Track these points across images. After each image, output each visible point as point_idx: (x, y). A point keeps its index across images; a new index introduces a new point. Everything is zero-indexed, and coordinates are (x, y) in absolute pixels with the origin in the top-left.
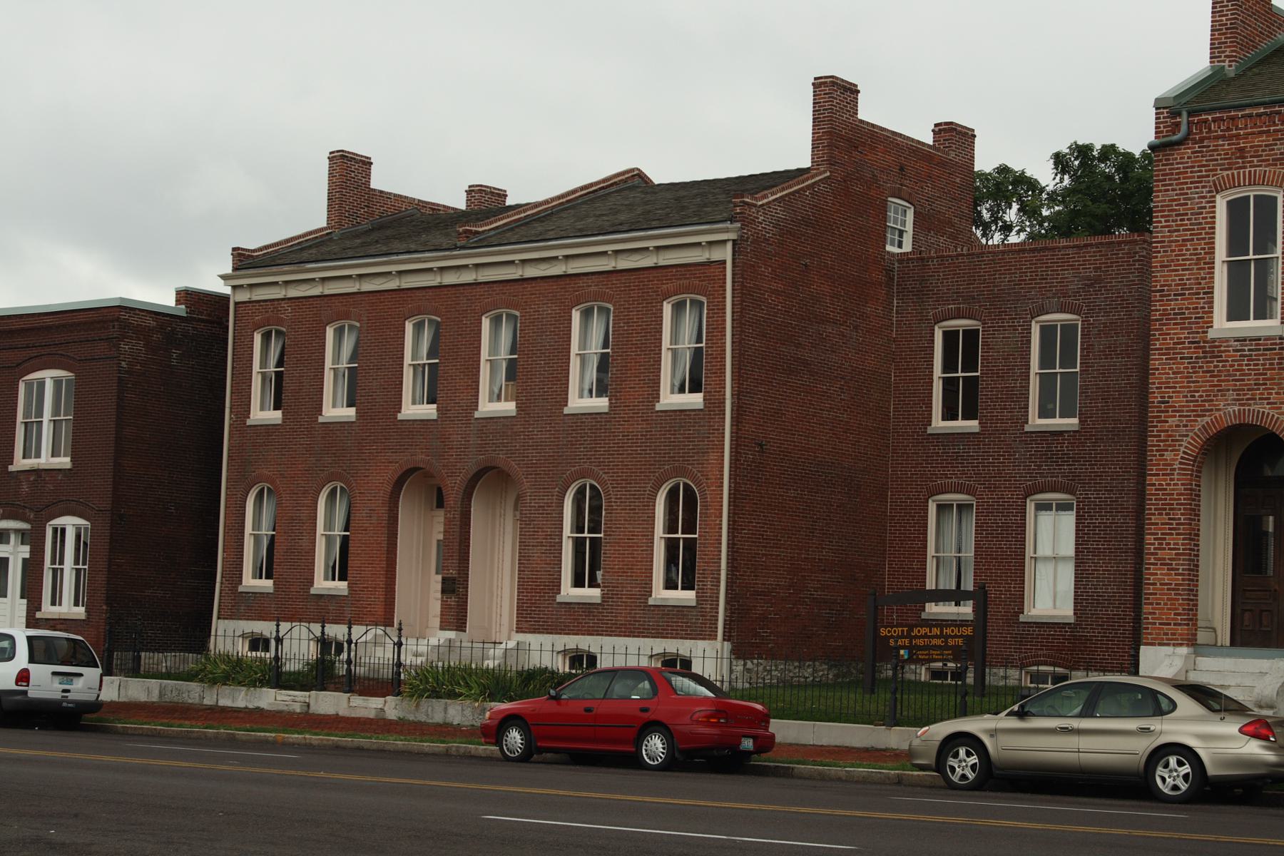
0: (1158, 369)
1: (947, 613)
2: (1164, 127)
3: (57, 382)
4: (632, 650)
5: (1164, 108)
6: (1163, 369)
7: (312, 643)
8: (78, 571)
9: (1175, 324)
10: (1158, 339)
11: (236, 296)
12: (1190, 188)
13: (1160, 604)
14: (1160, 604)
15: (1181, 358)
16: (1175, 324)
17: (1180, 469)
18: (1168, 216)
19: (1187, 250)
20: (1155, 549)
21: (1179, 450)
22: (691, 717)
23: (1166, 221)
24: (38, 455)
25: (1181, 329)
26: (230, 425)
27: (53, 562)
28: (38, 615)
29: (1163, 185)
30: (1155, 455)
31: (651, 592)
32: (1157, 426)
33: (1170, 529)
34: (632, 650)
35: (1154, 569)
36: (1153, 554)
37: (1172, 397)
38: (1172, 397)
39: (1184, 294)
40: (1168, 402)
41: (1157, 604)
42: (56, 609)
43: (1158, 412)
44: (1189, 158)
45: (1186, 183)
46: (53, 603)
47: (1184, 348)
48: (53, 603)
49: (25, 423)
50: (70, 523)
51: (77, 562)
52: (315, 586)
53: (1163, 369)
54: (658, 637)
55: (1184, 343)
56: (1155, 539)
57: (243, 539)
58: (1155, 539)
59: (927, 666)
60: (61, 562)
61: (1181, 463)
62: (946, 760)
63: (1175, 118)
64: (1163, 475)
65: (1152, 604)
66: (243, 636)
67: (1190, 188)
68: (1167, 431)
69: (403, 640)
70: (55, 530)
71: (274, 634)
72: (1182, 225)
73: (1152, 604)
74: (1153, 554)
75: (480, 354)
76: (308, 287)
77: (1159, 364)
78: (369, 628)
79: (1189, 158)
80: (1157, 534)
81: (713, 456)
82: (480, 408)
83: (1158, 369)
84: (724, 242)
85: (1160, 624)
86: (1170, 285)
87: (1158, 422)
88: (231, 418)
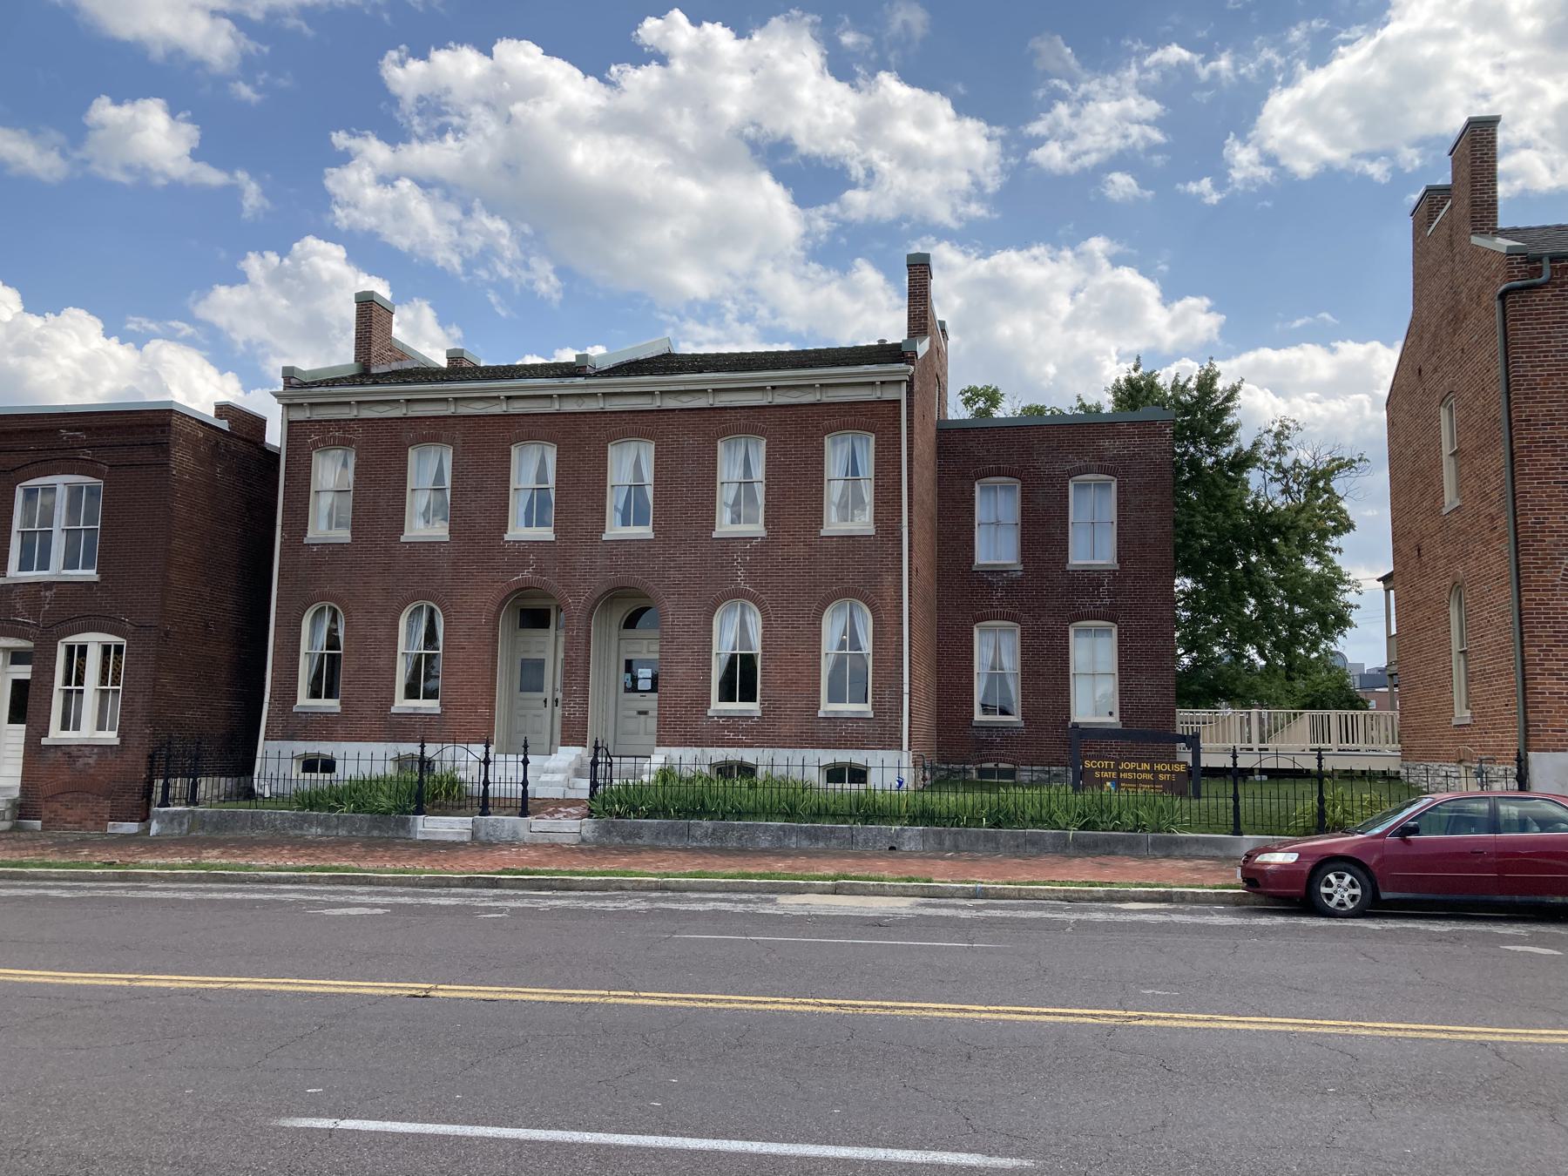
0: (1529, 492)
1: (1100, 724)
2: (1519, 272)
3: (75, 492)
4: (365, 754)
5: (1517, 254)
6: (1535, 492)
7: (294, 761)
8: (104, 693)
9: (1545, 451)
10: (1528, 465)
11: (291, 413)
12: (1553, 328)
13: (1551, 712)
14: (1551, 712)
15: (1555, 483)
16: (1545, 451)
17: (1562, 585)
18: (1530, 352)
19: (1553, 384)
20: (1540, 660)
21: (1560, 568)
22: (1249, 856)
23: (1527, 357)
24: (44, 566)
25: (1553, 455)
26: (281, 543)
27: (68, 681)
28: (44, 741)
29: (1521, 324)
30: (1533, 573)
31: (819, 705)
32: (1533, 545)
33: (1556, 641)
34: (365, 754)
35: (1541, 679)
36: (1538, 665)
37: (1548, 518)
38: (1548, 518)
39: (1554, 424)
40: (1544, 523)
41: (1548, 712)
42: (65, 734)
43: (1532, 532)
44: (1549, 300)
45: (1548, 323)
46: (65, 727)
47: (1557, 473)
48: (65, 727)
49: (23, 532)
50: (94, 641)
51: (104, 681)
52: (396, 705)
53: (1535, 492)
54: (829, 748)
55: (1557, 469)
56: (1539, 651)
57: (298, 658)
58: (1539, 651)
59: (979, 766)
60: (80, 681)
61: (1562, 579)
62: (1351, 874)
63: (1534, 262)
64: (1544, 590)
65: (1542, 712)
66: (298, 758)
67: (1553, 328)
68: (1545, 550)
69: (491, 757)
70: (70, 649)
71: (801, 778)
72: (1546, 361)
73: (1542, 712)
74: (1538, 665)
75: (606, 479)
76: (388, 408)
77: (1531, 488)
78: (445, 745)
79: (1549, 300)
80: (1542, 646)
81: (889, 579)
82: (607, 530)
83: (1529, 492)
84: (900, 382)
85: (1553, 731)
86: (1538, 416)
87: (1534, 541)
88: (282, 537)
